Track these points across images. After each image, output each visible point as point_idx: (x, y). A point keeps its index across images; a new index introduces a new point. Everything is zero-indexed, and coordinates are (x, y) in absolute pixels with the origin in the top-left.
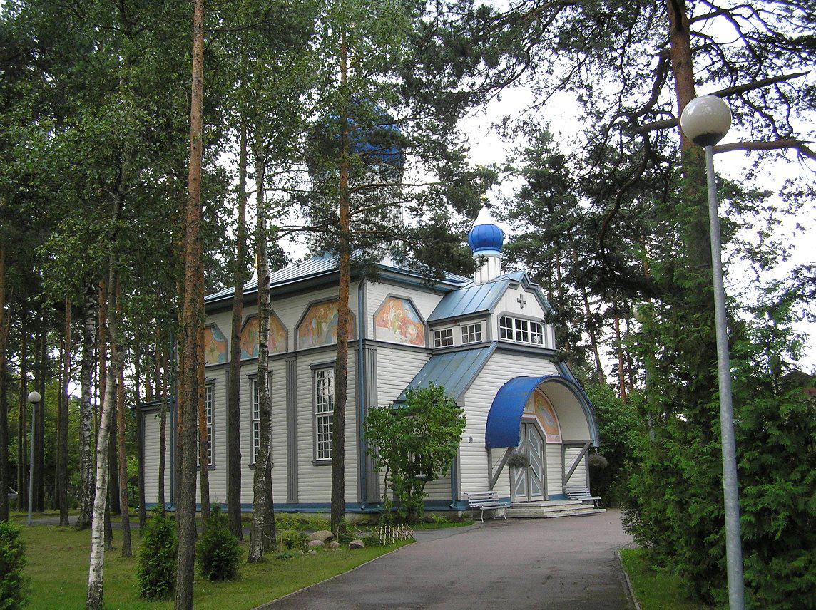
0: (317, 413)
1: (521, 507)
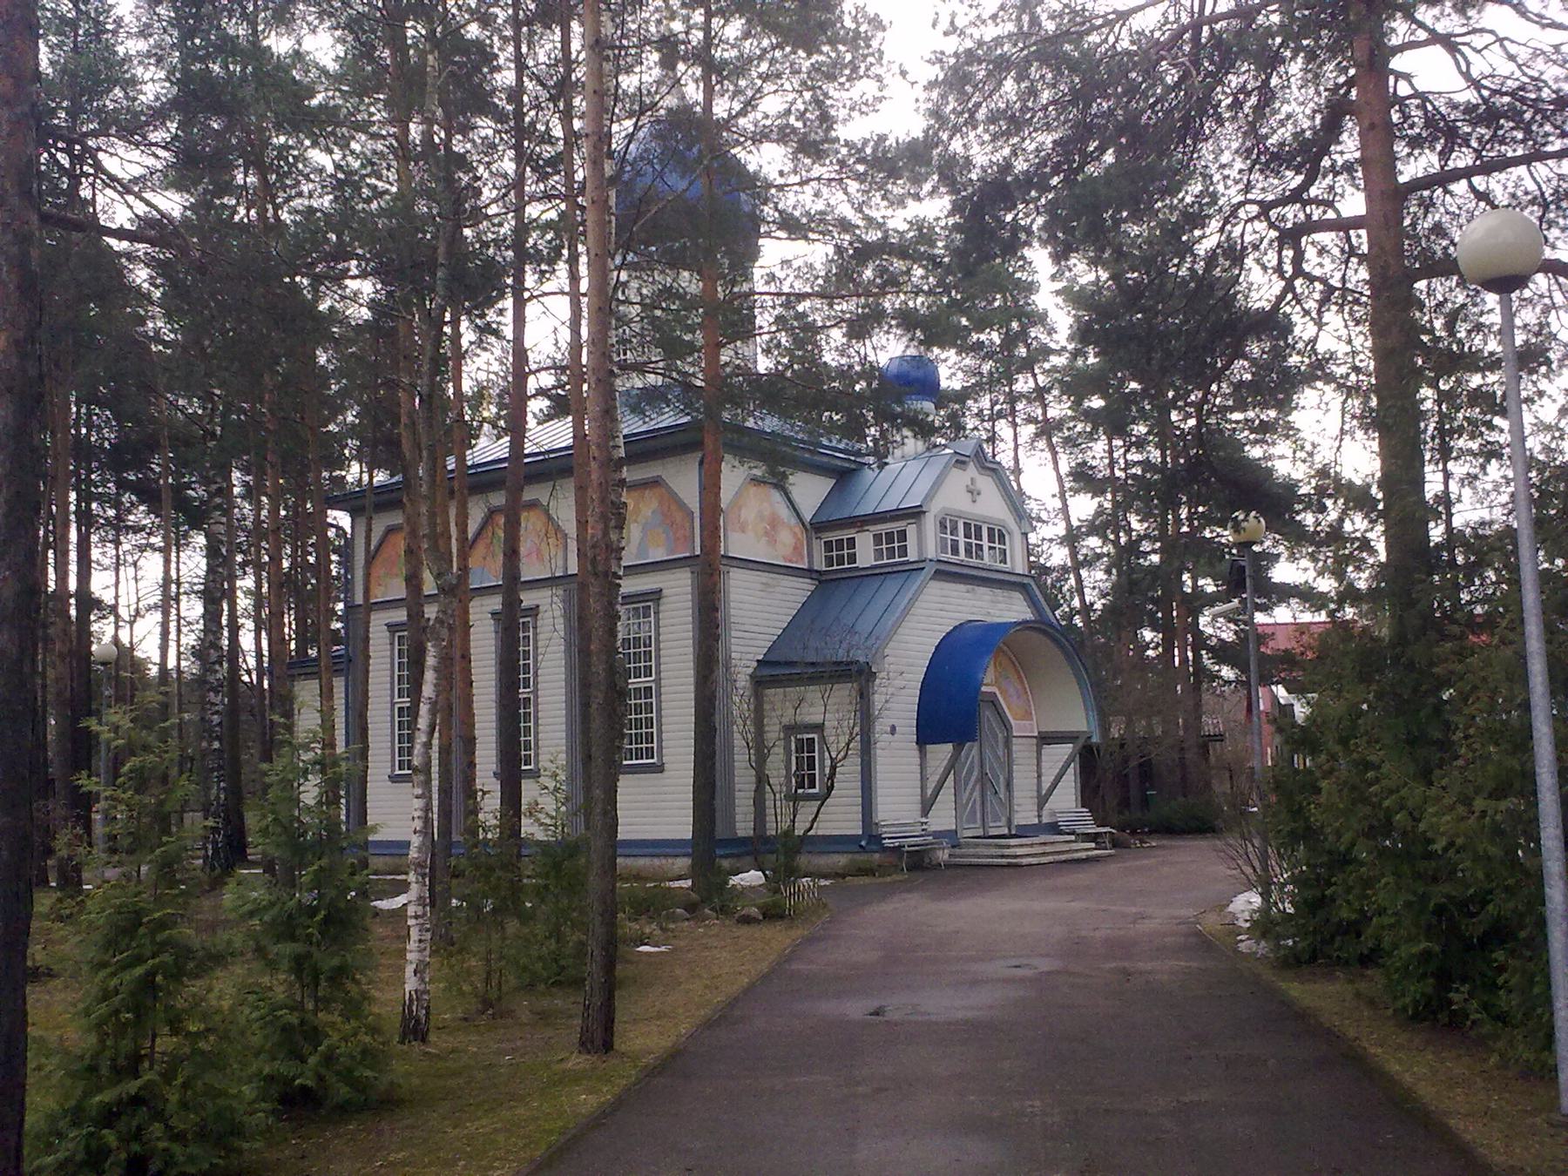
0: (397, 700)
1: (977, 845)
